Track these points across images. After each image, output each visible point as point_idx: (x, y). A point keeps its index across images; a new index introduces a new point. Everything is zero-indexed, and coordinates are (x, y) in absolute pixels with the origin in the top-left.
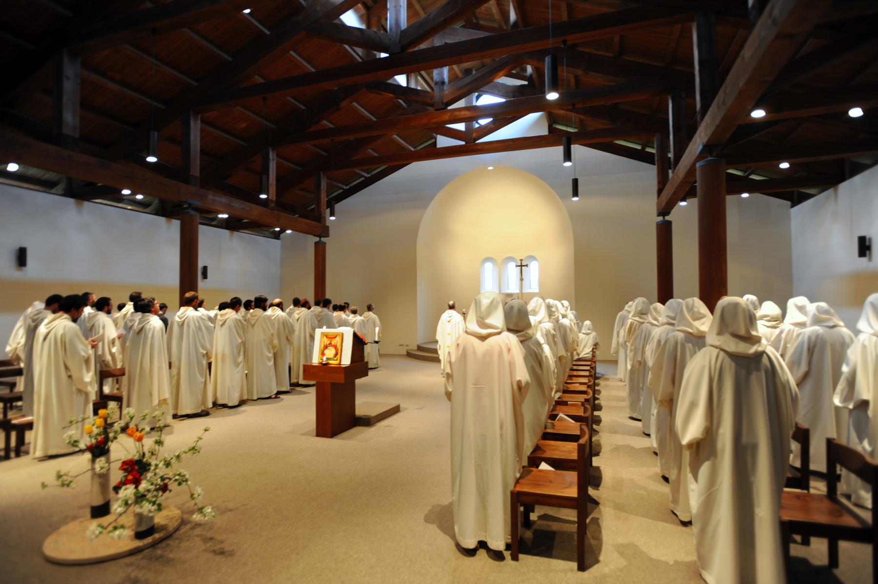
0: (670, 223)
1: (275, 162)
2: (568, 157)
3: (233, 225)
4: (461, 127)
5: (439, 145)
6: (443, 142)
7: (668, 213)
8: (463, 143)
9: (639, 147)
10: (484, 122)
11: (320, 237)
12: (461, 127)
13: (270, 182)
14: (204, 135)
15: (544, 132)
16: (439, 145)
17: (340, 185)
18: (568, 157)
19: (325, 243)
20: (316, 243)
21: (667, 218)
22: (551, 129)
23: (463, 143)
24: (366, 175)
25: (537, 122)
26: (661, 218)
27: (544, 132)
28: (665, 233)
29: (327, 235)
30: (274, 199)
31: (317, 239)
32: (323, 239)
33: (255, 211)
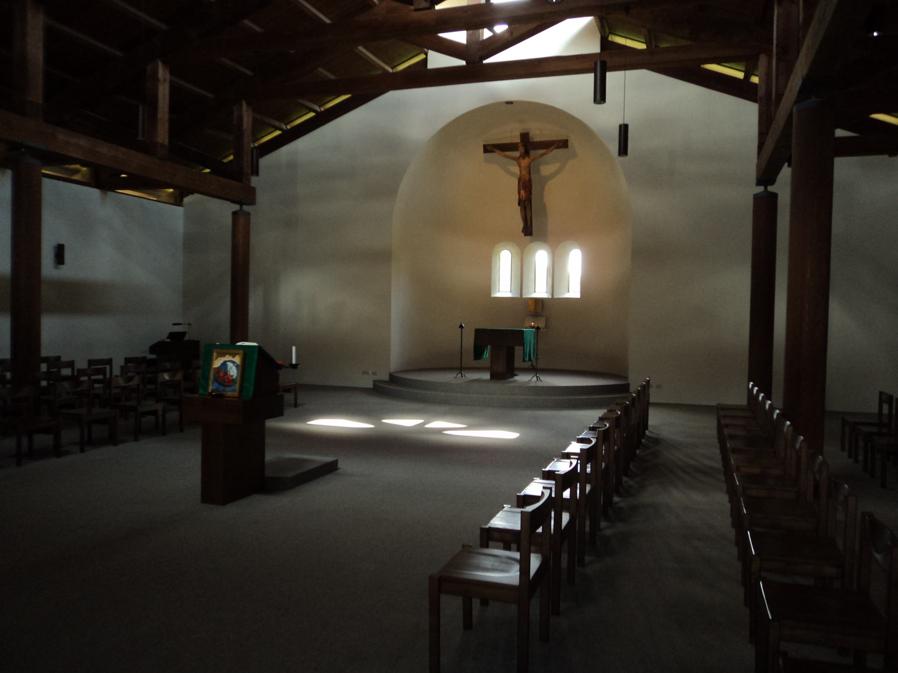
0: (759, 183)
1: (167, 85)
2: (600, 95)
3: (105, 180)
4: (460, 37)
5: (431, 66)
6: (437, 60)
7: (772, 182)
8: (463, 63)
9: (740, 75)
10: (501, 29)
11: (241, 203)
12: (460, 37)
13: (160, 115)
14: (51, 38)
15: (594, 48)
16: (431, 66)
17: (277, 123)
18: (600, 95)
19: (249, 214)
20: (235, 214)
21: (771, 189)
22: (605, 44)
23: (463, 63)
24: (318, 109)
25: (584, 33)
26: (761, 189)
27: (594, 48)
28: (765, 206)
29: (252, 202)
30: (166, 142)
31: (236, 207)
32: (245, 208)
33: (136, 160)
